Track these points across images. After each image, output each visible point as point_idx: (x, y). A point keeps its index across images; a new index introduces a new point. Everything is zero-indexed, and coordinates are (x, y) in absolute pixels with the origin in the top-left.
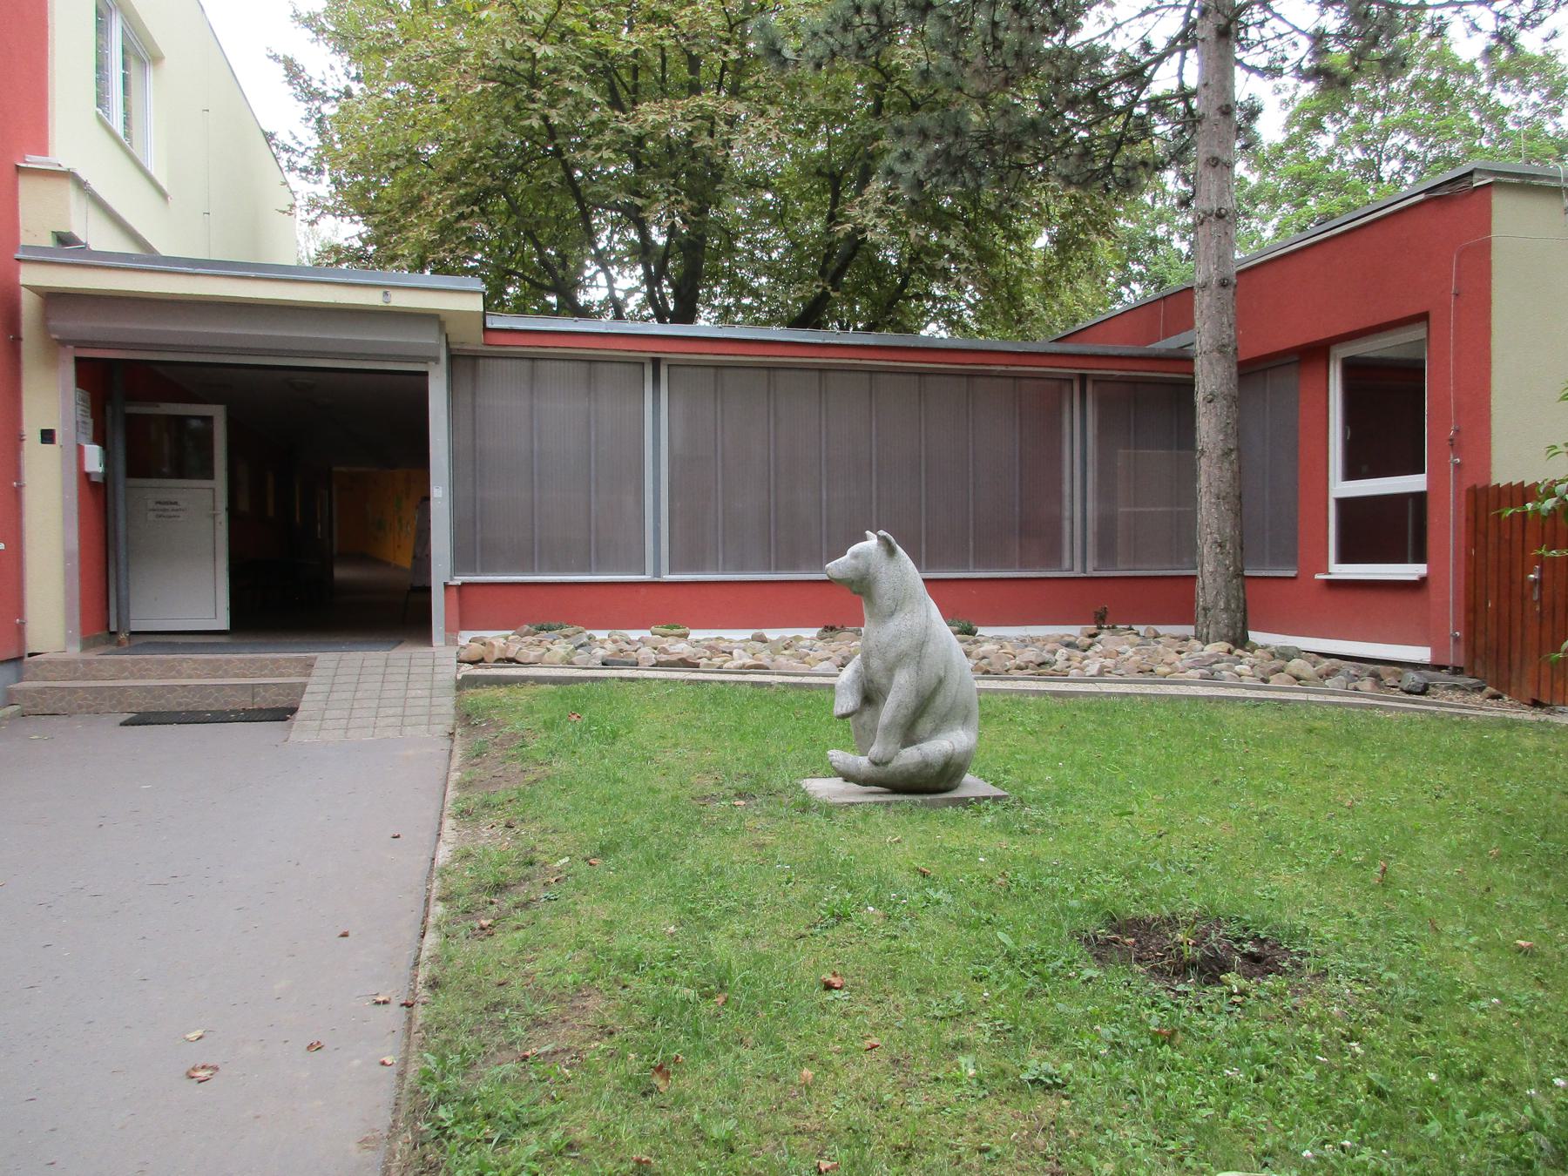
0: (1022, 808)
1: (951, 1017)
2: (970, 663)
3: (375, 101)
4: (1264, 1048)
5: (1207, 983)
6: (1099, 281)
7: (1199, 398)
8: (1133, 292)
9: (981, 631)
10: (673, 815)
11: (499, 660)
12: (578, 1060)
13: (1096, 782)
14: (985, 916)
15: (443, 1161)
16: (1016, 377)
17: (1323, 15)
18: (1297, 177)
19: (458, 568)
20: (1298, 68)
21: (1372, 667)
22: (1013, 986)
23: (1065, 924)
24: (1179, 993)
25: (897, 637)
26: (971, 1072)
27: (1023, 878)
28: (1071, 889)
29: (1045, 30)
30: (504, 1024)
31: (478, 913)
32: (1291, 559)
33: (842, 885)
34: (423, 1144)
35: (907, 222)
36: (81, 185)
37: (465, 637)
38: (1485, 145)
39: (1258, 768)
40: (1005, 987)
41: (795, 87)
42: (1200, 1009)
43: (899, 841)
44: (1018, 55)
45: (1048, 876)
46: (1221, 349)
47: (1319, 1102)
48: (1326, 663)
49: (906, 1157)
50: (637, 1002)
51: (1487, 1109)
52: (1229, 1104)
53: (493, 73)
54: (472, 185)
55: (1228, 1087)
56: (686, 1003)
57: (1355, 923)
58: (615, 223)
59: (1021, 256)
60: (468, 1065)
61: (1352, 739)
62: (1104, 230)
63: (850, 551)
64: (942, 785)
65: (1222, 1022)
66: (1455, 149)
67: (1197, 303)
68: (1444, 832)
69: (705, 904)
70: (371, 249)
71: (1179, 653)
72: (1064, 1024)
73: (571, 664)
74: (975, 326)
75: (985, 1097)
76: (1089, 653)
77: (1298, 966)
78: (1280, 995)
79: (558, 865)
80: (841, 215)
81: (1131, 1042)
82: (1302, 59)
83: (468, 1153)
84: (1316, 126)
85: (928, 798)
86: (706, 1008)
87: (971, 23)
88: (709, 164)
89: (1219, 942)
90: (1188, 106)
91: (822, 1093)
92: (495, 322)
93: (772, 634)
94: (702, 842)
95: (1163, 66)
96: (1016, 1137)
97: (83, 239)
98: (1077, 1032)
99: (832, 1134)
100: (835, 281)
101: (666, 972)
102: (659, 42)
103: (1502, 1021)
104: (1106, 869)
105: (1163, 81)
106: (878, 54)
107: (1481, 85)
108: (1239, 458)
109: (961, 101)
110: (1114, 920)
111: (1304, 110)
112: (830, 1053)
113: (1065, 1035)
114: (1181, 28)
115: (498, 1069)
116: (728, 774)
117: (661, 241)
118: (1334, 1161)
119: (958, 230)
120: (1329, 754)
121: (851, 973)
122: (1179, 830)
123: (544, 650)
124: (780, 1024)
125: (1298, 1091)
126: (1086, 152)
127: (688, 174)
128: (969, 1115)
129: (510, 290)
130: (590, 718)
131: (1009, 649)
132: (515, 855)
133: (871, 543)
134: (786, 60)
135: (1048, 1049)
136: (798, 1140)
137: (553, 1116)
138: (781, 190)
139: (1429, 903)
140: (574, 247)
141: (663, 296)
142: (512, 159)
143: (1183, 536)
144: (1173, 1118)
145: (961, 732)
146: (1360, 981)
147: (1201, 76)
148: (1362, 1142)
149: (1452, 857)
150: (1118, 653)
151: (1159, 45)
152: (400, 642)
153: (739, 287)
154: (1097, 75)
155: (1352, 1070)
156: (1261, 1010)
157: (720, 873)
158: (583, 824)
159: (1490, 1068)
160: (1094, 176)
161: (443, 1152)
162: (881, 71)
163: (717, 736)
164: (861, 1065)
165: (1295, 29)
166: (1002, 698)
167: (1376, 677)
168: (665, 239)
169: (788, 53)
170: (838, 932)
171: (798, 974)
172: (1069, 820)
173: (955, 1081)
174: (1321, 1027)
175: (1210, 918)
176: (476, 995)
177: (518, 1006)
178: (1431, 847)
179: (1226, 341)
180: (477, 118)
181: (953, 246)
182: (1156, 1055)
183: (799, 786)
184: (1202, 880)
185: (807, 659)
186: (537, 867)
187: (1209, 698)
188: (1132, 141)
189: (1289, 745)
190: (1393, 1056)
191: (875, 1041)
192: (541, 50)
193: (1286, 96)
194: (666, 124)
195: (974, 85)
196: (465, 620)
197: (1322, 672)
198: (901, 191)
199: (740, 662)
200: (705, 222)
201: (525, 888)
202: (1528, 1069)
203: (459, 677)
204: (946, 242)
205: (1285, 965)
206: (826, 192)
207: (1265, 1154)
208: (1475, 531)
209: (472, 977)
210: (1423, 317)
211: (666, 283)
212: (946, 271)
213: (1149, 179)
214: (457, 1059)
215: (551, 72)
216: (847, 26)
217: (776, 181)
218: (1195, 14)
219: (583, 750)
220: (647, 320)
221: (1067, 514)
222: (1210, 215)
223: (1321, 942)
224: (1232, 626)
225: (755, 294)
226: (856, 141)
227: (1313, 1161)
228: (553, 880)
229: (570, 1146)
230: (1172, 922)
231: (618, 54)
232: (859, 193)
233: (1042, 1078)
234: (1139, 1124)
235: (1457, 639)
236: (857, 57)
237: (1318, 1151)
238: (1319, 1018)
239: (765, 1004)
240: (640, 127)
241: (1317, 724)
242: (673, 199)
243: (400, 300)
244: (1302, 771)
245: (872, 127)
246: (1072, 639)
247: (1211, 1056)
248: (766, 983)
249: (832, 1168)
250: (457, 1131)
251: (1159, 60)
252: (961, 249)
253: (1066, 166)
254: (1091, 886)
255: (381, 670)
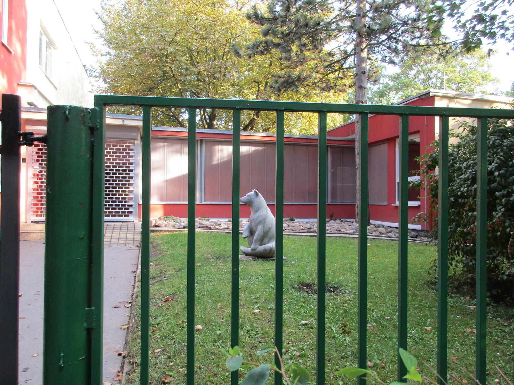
9: (296, 220)
25: (258, 217)
36: (35, 88)
48: (390, 229)
64: (270, 256)
71: (349, 226)
97: (36, 104)
133: (252, 193)
243: (127, 123)
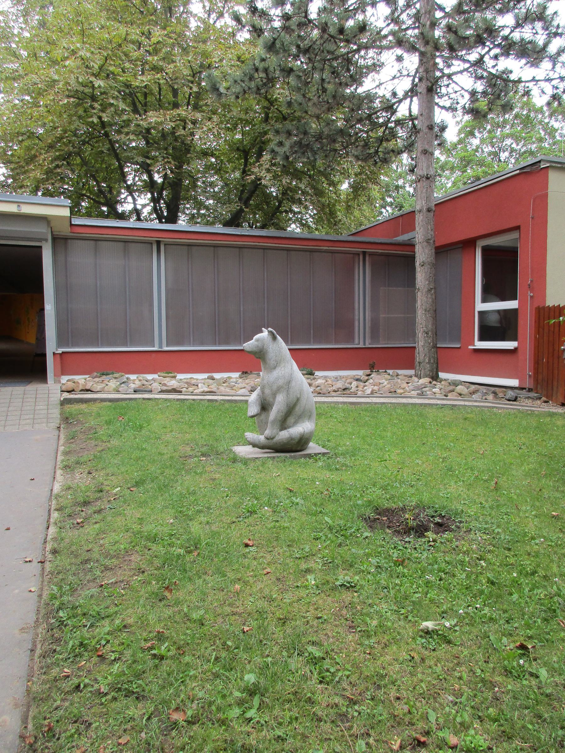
0: (336, 457)
1: (304, 557)
2: (312, 389)
3: (10, 105)
4: (443, 565)
5: (419, 537)
6: (373, 206)
7: (417, 264)
8: (387, 211)
9: (318, 373)
10: (171, 466)
11: (82, 390)
12: (128, 585)
13: (370, 445)
14: (319, 510)
15: (62, 637)
16: (333, 252)
17: (475, 83)
18: (462, 159)
19: (59, 344)
20: (464, 108)
21: (493, 389)
22: (332, 542)
23: (356, 512)
24: (406, 542)
25: (277, 379)
26: (313, 582)
27: (336, 491)
28: (358, 495)
29: (347, 85)
30: (91, 570)
31: (75, 516)
32: (458, 339)
33: (252, 497)
34: (52, 629)
35: (281, 175)
37: (64, 379)
38: (547, 146)
39: (442, 437)
40: (328, 542)
41: (225, 106)
42: (415, 549)
43: (279, 475)
44: (334, 97)
45: (348, 490)
46: (428, 241)
47: (467, 588)
48: (473, 387)
49: (284, 623)
50: (156, 557)
51: (538, 588)
52: (428, 591)
53: (72, 93)
54: (63, 150)
55: (428, 582)
56: (179, 556)
57: (484, 507)
58: (136, 171)
59: (335, 193)
60: (73, 590)
61: (484, 422)
62: (376, 182)
63: (256, 337)
64: (299, 448)
65: (425, 554)
66: (534, 147)
67: (417, 219)
68: (522, 464)
69: (187, 508)
70: (10, 181)
71: (408, 383)
72: (355, 558)
73: (118, 391)
74: (314, 226)
75: (319, 593)
76: (366, 384)
77: (459, 527)
78: (451, 541)
79: (115, 491)
80: (249, 170)
81: (385, 565)
82: (466, 104)
83: (75, 632)
84: (472, 134)
85: (292, 454)
86: (191, 557)
87: (312, 79)
88: (183, 142)
89: (424, 518)
90: (413, 124)
91: (244, 595)
92: (76, 221)
93: (217, 376)
94: (185, 478)
95: (402, 104)
96: (333, 611)
98: (361, 562)
99: (249, 614)
100: (246, 203)
101: (169, 542)
102: (158, 81)
103: (545, 549)
104: (374, 486)
105: (402, 111)
106: (266, 92)
107: (545, 118)
108: (435, 293)
109: (307, 117)
110: (378, 509)
111: (467, 127)
112: (248, 577)
113: (355, 563)
114: (410, 87)
115: (88, 592)
116: (197, 445)
117: (160, 181)
118: (472, 614)
119: (305, 181)
120: (473, 429)
121: (257, 538)
122: (407, 466)
123: (104, 385)
124: (224, 564)
125: (458, 584)
126: (366, 145)
127: (173, 148)
128: (312, 602)
129: (83, 204)
130: (128, 419)
131: (330, 382)
132: (93, 487)
133: (265, 334)
134: (221, 93)
135: (348, 570)
136: (233, 618)
137: (116, 613)
138: (219, 157)
139: (515, 497)
140: (115, 183)
141: (161, 208)
142: (83, 138)
143: (411, 333)
144: (403, 599)
145: (307, 423)
146: (485, 533)
147: (419, 110)
148: (484, 605)
149: (525, 475)
150: (380, 383)
151: (400, 94)
152: (31, 382)
153: (199, 205)
154: (371, 107)
155: (481, 573)
156: (442, 548)
157: (194, 493)
158: (127, 471)
159: (539, 570)
160: (369, 156)
161: (63, 632)
162: (268, 100)
163: (191, 427)
164: (262, 582)
165: (463, 89)
166: (327, 405)
167: (495, 393)
168: (162, 180)
169: (222, 90)
170: (250, 520)
171: (232, 540)
172: (357, 463)
173: (306, 587)
174: (468, 555)
175: (421, 507)
176: (76, 556)
177: (97, 561)
178: (517, 471)
179: (430, 237)
180: (65, 116)
181: (303, 188)
182: (396, 570)
183: (231, 450)
184: (417, 489)
185: (234, 388)
186: (104, 493)
187: (421, 405)
188: (388, 140)
189: (456, 426)
190: (498, 566)
191: (268, 570)
192: (98, 83)
193: (458, 119)
194: (161, 123)
195: (312, 110)
196: (64, 371)
197: (471, 391)
198: (278, 160)
199: (202, 390)
200: (182, 173)
201: (99, 503)
202: (555, 569)
203: (62, 399)
204: (300, 185)
205: (453, 527)
206: (241, 159)
207: (443, 613)
208: (539, 327)
209: (74, 548)
210: (518, 228)
211: (162, 202)
212: (300, 199)
213: (396, 157)
214: (68, 587)
215: (102, 94)
216: (251, 78)
217: (217, 153)
218: (417, 80)
219: (126, 434)
220: (152, 220)
221: (357, 317)
222: (423, 177)
223: (469, 516)
224: (431, 371)
225: (207, 208)
226: (256, 134)
227: (463, 614)
228: (112, 499)
229: (125, 627)
230: (403, 510)
231: (138, 87)
232: (258, 161)
233: (345, 583)
234: (388, 602)
235: (530, 376)
236: (257, 94)
237: (466, 610)
238: (467, 551)
239: (217, 555)
240: (149, 124)
241: (469, 416)
242: (166, 160)
243: (27, 210)
244: (461, 438)
245: (263, 128)
246: (359, 377)
247: (420, 570)
248: (217, 545)
249: (250, 630)
250: (69, 622)
251: (400, 101)
252: (308, 189)
253: (357, 151)
254: (367, 494)
255: (21, 396)
